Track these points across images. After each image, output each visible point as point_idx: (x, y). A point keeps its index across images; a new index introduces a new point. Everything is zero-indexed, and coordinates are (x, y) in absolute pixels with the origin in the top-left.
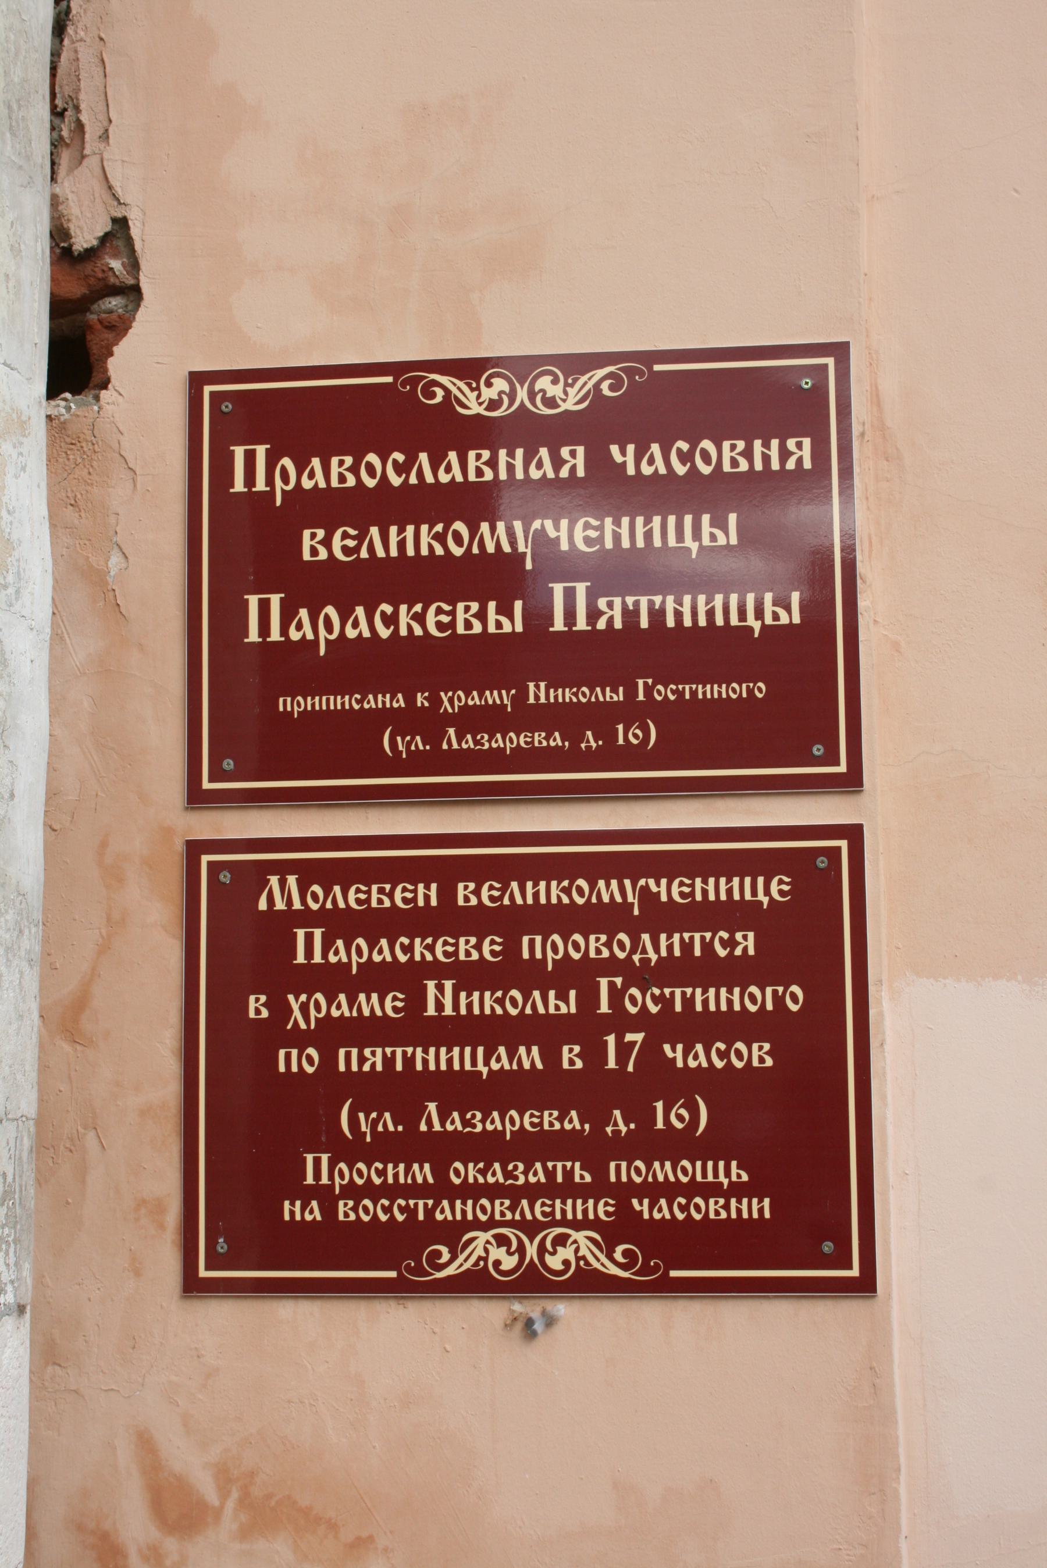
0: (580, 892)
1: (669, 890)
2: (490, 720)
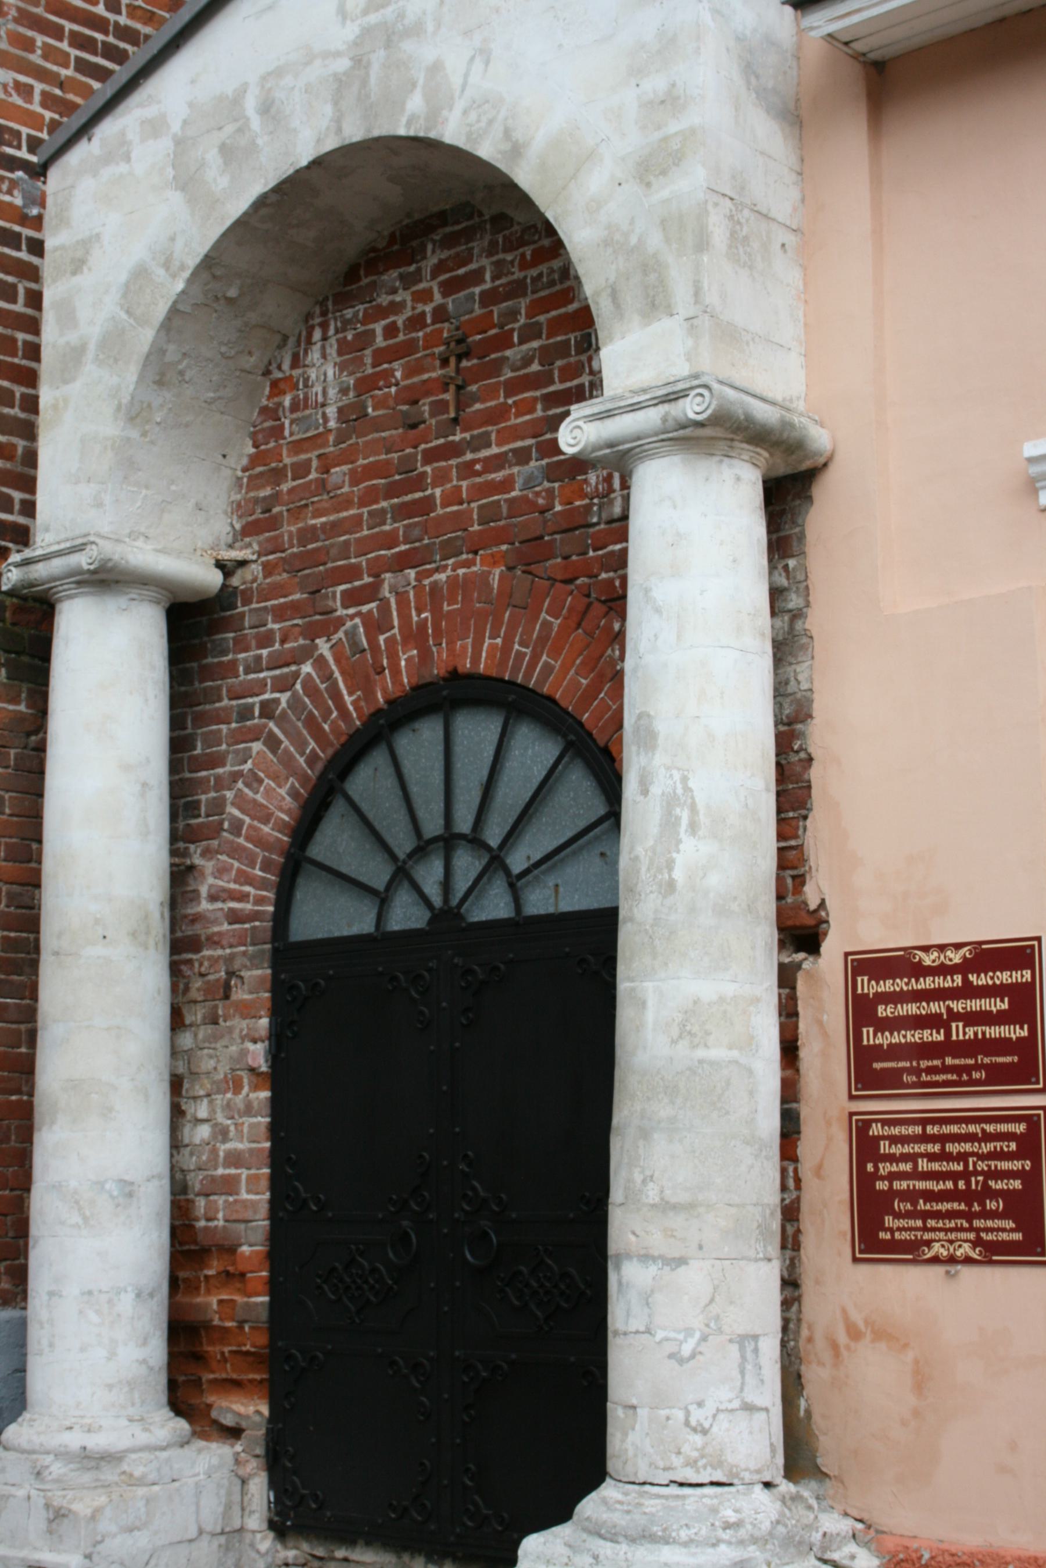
1: (990, 1128)
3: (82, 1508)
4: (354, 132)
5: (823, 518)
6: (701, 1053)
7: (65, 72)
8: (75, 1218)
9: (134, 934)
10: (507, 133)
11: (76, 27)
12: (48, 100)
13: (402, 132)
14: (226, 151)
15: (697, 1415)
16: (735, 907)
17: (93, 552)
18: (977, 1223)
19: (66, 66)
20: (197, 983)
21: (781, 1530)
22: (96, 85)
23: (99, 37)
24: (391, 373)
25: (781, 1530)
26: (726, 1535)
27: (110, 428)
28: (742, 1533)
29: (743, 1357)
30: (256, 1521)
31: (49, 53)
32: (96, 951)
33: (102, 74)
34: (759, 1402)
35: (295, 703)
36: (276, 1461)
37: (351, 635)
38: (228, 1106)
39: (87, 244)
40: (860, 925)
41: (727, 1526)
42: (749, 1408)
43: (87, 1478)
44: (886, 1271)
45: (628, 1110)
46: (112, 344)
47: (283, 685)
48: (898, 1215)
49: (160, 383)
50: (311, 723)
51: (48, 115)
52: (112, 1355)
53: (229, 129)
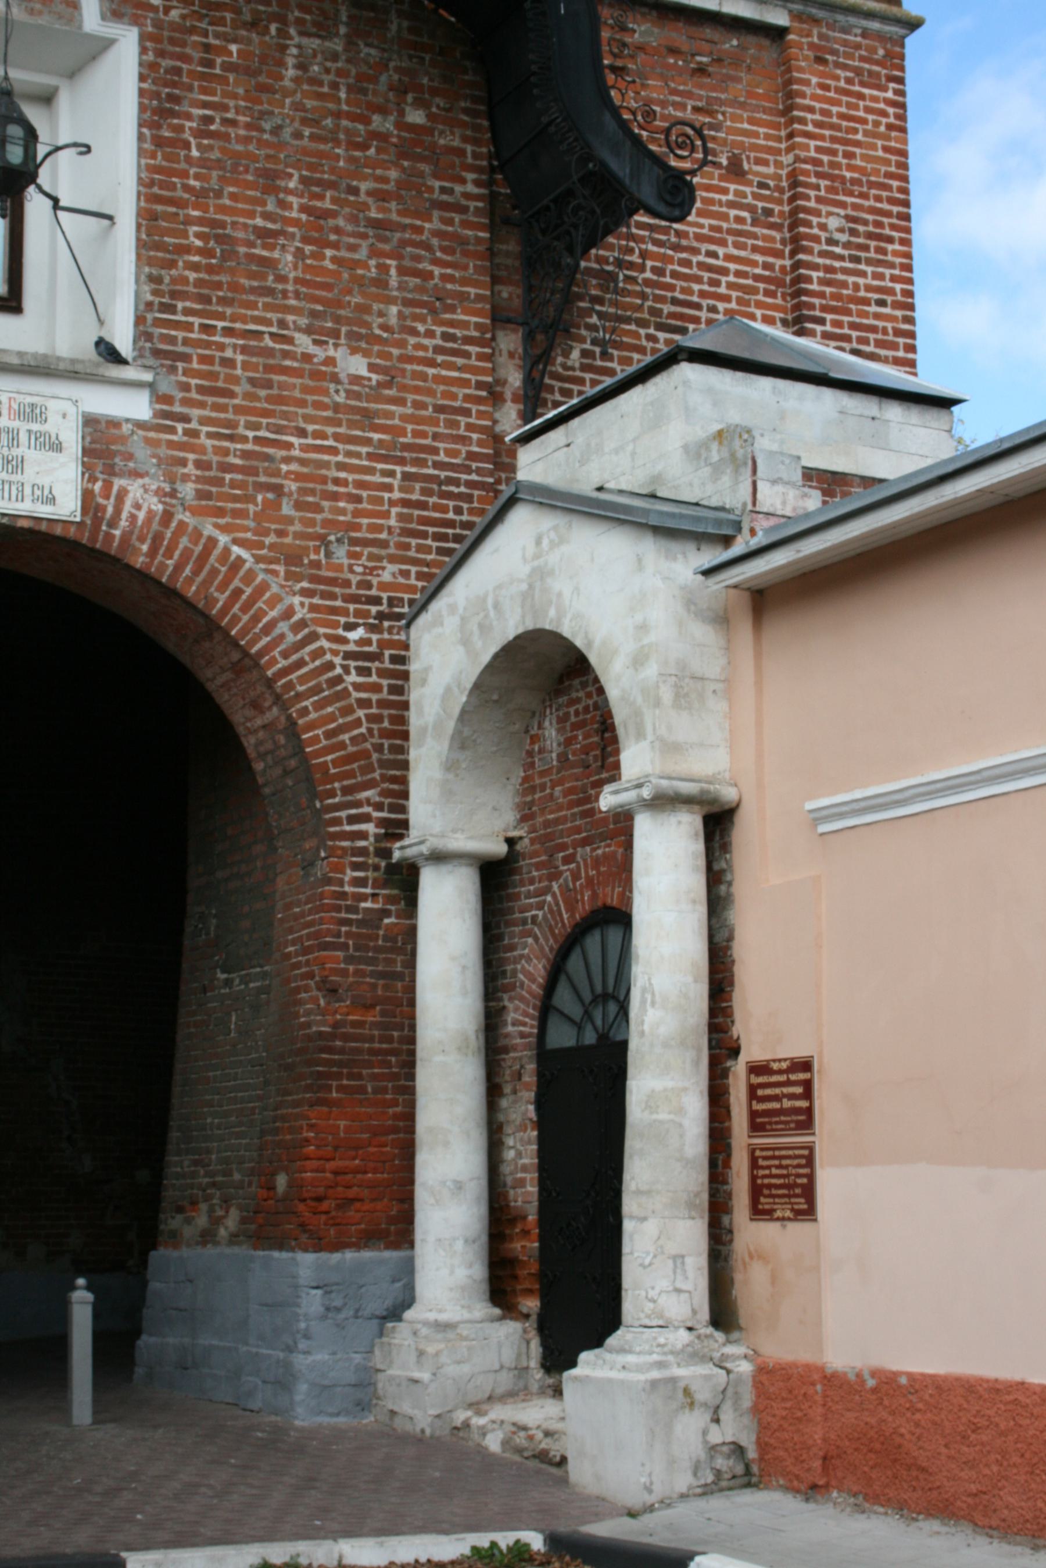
0: (790, 1152)
1: (777, 1153)
2: (777, 1123)
3: (431, 1349)
4: (530, 626)
5: (745, 833)
6: (655, 1116)
7: (429, 557)
8: (432, 1201)
9: (459, 1049)
10: (586, 637)
11: (436, 529)
12: (420, 576)
13: (547, 627)
14: (481, 626)
15: (652, 1294)
16: (673, 1043)
17: (428, 844)
18: (793, 1200)
19: (430, 553)
20: (508, 1072)
21: (690, 1349)
22: (447, 559)
23: (450, 531)
24: (576, 737)
25: (690, 1349)
26: (658, 1350)
27: (438, 774)
28: (666, 1349)
29: (675, 1266)
30: (534, 1363)
31: (420, 549)
32: (439, 1058)
33: (449, 552)
34: (684, 1287)
35: (545, 916)
36: (542, 1329)
37: (566, 880)
38: (521, 1140)
39: (427, 669)
40: (752, 1051)
41: (659, 1345)
42: (678, 1291)
43: (440, 1336)
44: (762, 1224)
45: (632, 1143)
46: (438, 725)
47: (540, 906)
48: (766, 1196)
49: (463, 747)
50: (551, 929)
51: (420, 584)
52: (452, 1272)
53: (482, 615)
